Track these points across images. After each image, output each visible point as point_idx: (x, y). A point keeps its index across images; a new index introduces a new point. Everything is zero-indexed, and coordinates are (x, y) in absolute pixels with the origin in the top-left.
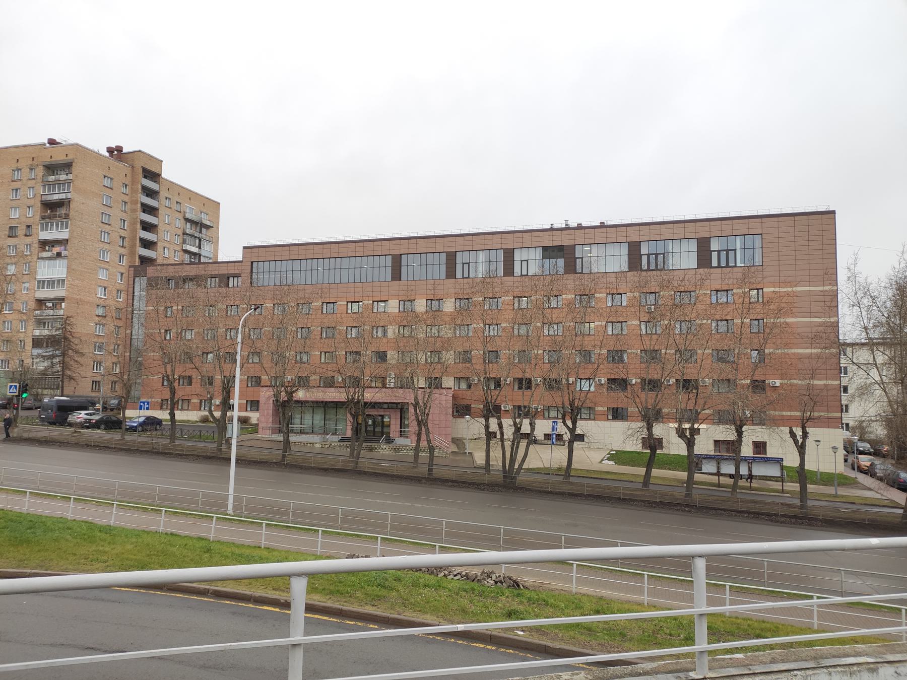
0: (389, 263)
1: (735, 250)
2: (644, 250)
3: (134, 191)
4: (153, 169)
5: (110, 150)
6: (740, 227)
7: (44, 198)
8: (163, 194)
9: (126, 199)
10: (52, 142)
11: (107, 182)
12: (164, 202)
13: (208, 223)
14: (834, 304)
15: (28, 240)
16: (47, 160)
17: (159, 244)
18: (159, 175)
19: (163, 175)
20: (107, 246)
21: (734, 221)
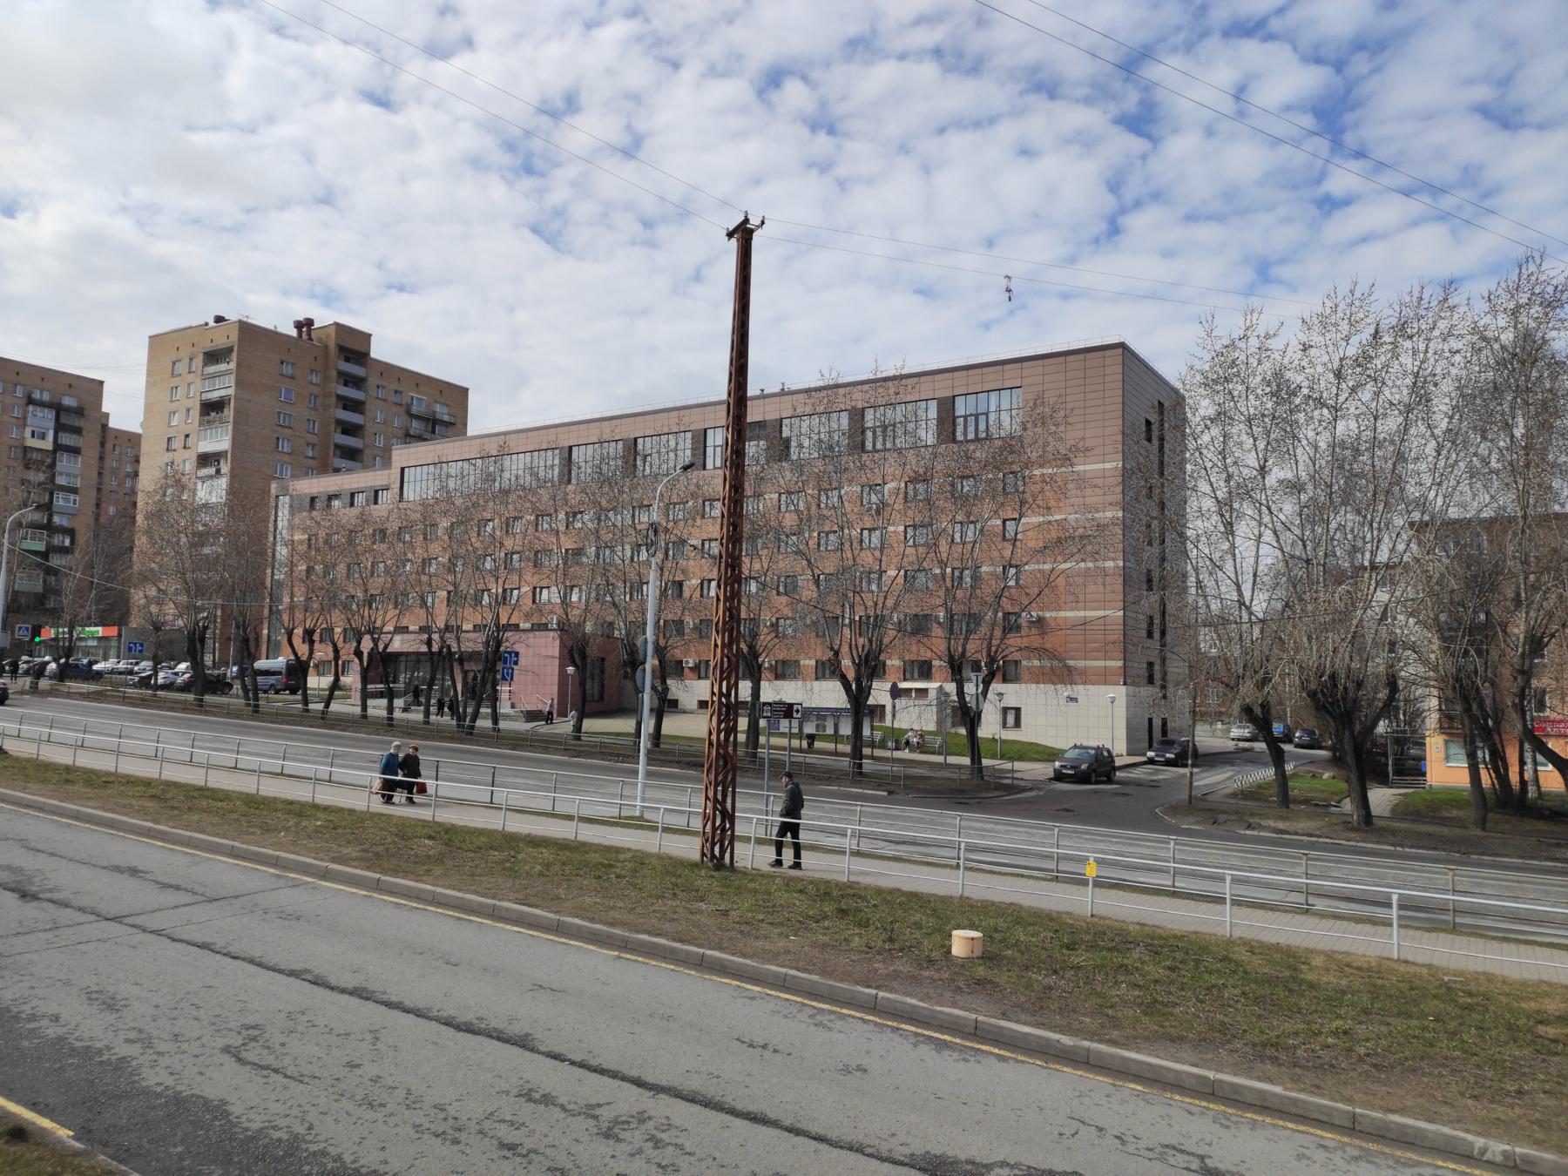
0: (933, 413)
1: (987, 414)
2: (960, 410)
3: (326, 379)
4: (357, 347)
5: (299, 325)
6: (991, 379)
7: (204, 396)
8: (373, 381)
9: (316, 390)
10: (219, 319)
11: (287, 370)
12: (373, 392)
13: (446, 418)
14: (966, 922)
15: (187, 454)
16: (208, 346)
17: (367, 452)
18: (367, 354)
19: (374, 354)
20: (287, 458)
21: (985, 370)
